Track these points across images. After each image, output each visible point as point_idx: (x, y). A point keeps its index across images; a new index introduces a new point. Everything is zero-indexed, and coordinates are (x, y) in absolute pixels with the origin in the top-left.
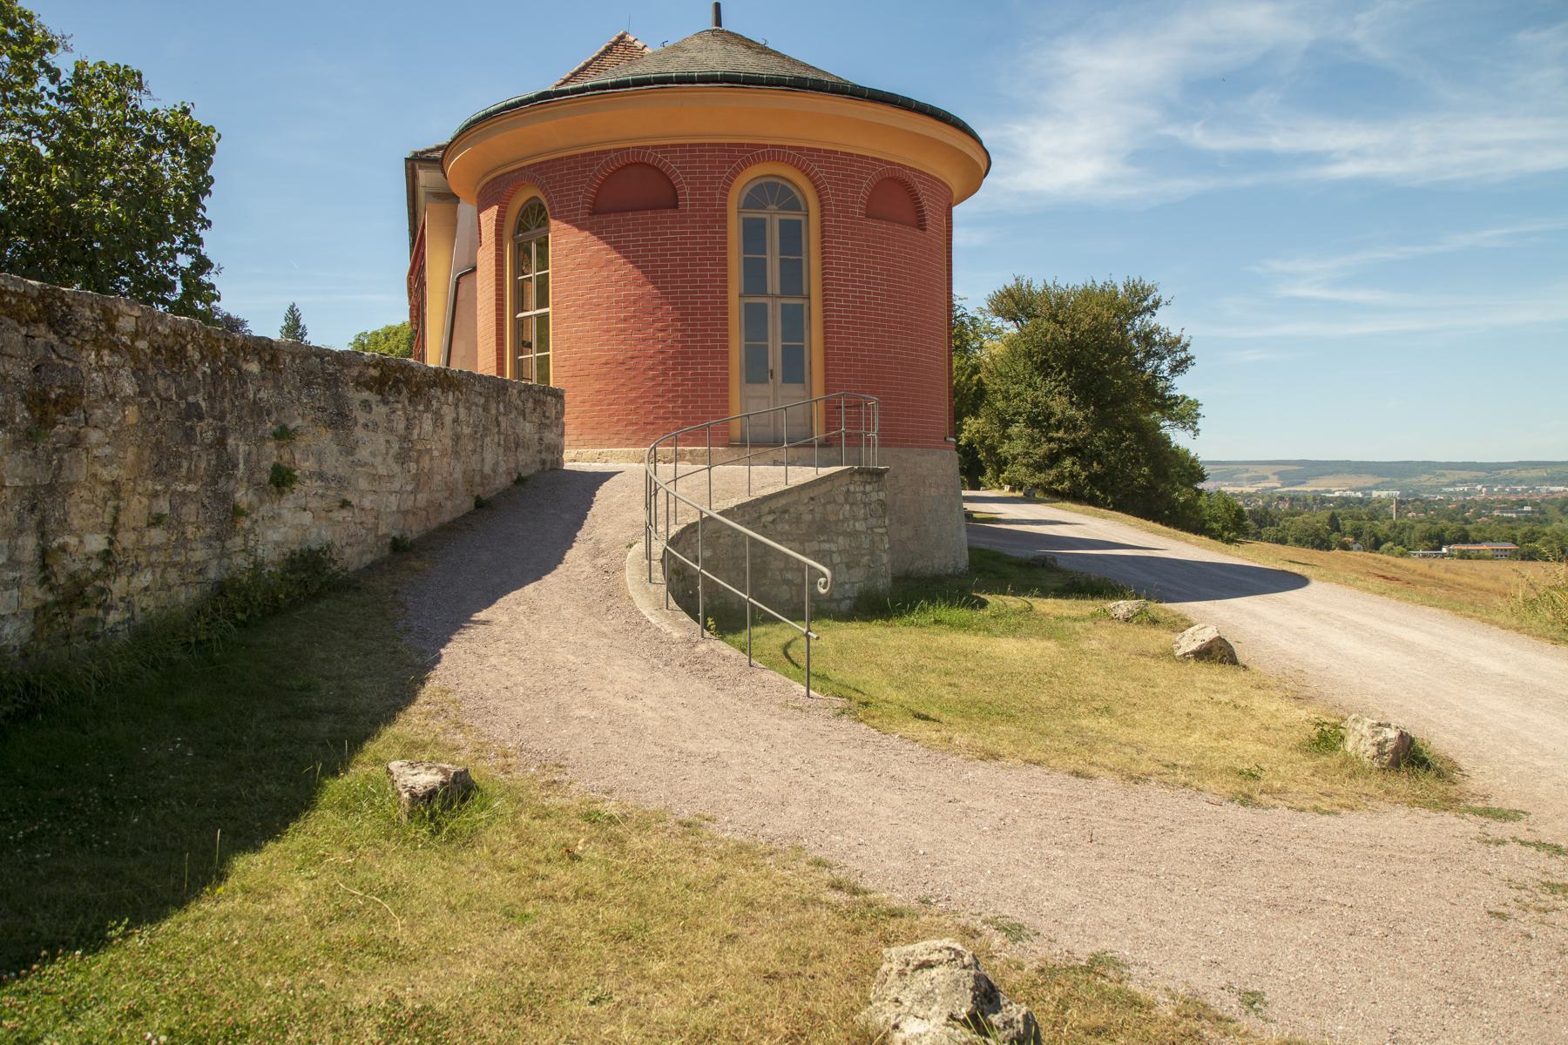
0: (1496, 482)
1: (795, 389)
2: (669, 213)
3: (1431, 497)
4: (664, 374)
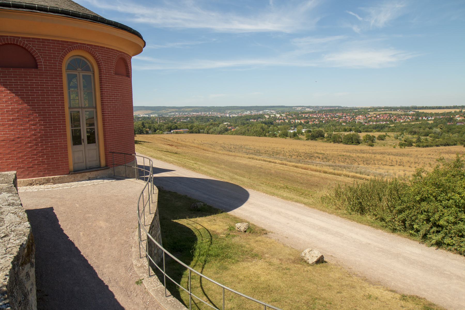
1: (92, 146)
2: (33, 70)
3: (165, 116)
4: (37, 145)
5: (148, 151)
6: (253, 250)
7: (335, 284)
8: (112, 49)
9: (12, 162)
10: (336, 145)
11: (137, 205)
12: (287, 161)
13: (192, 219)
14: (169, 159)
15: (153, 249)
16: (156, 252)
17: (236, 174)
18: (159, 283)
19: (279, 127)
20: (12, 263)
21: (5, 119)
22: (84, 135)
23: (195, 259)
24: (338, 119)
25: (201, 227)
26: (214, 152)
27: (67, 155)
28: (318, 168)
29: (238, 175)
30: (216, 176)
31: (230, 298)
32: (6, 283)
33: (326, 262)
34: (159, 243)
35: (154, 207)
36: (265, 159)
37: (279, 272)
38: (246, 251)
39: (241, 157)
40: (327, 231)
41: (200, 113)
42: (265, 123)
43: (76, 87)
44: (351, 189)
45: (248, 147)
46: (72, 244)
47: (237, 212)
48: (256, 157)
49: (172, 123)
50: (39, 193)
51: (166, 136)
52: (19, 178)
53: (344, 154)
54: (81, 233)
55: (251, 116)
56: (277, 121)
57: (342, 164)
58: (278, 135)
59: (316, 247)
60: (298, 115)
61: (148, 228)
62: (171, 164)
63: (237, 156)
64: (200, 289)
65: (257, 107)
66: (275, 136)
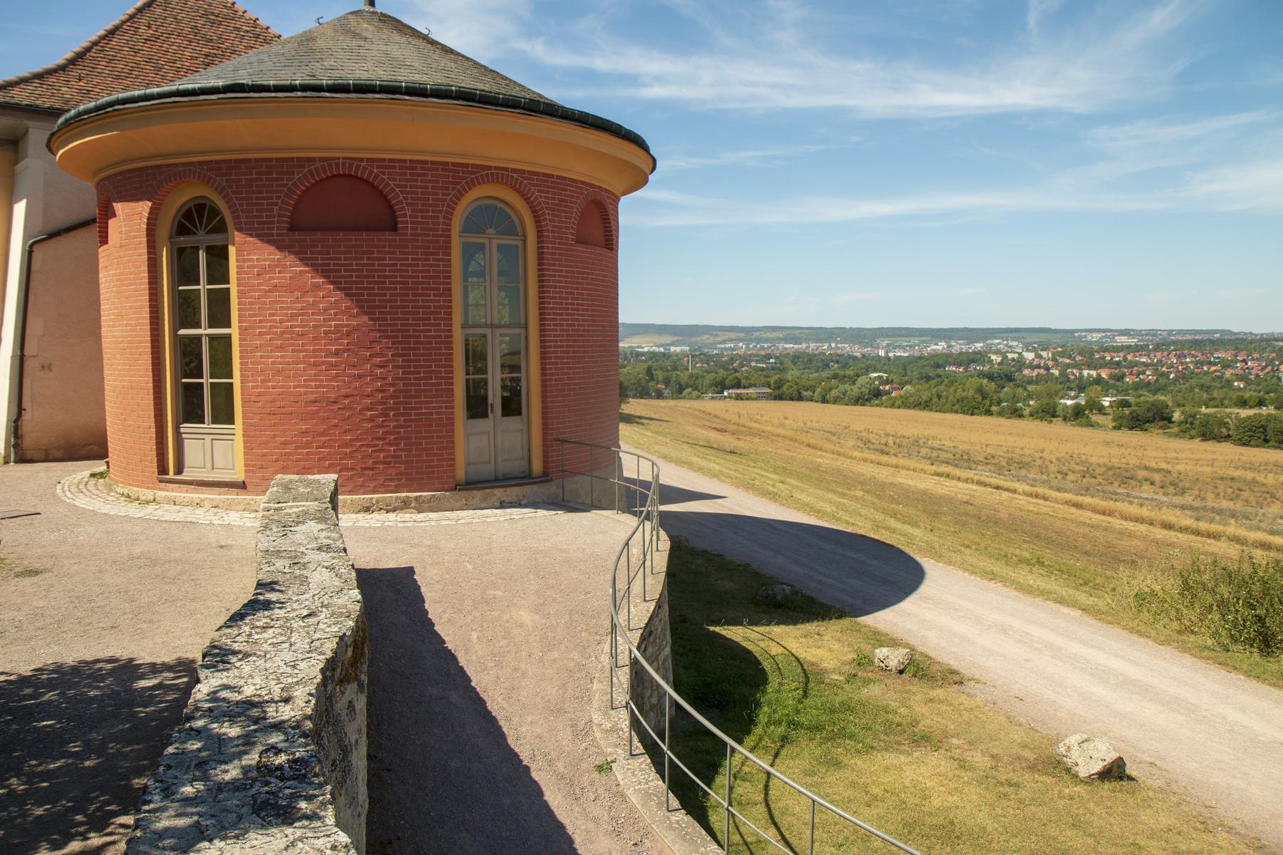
0: (751, 340)
1: (513, 422)
2: (387, 235)
5: (657, 443)
6: (918, 723)
7: (1154, 843)
8: (570, 180)
9: (329, 454)
10: (1211, 446)
11: (609, 577)
12: (1051, 488)
13: (756, 629)
14: (712, 465)
15: (648, 693)
16: (654, 700)
17: (894, 515)
18: (653, 775)
19: (1030, 388)
20: (322, 671)
21: (320, 350)
22: (495, 395)
23: (758, 730)
24: (1219, 367)
25: (780, 650)
26: (839, 454)
27: (453, 442)
28: (1145, 512)
29: (898, 520)
30: (833, 517)
31: (840, 840)
32: (309, 711)
33: (1131, 778)
34: (665, 678)
35: (656, 585)
36: (983, 479)
37: (987, 788)
38: (898, 725)
39: (914, 470)
40: (1144, 691)
41: (804, 346)
42: (991, 377)
43: (481, 274)
44: (1229, 576)
45: (936, 444)
46: (452, 657)
47: (883, 619)
48: (957, 472)
49: (727, 370)
50: (388, 532)
51: (710, 405)
52: (343, 493)
53: (1236, 474)
54: (474, 635)
55: (950, 355)
56: (1026, 372)
57: (1226, 504)
58: (1027, 412)
59: (1105, 734)
60: (1090, 355)
61: (635, 637)
62: (715, 480)
63: (903, 468)
64: (762, 808)
65: (966, 330)
66: (1017, 414)
